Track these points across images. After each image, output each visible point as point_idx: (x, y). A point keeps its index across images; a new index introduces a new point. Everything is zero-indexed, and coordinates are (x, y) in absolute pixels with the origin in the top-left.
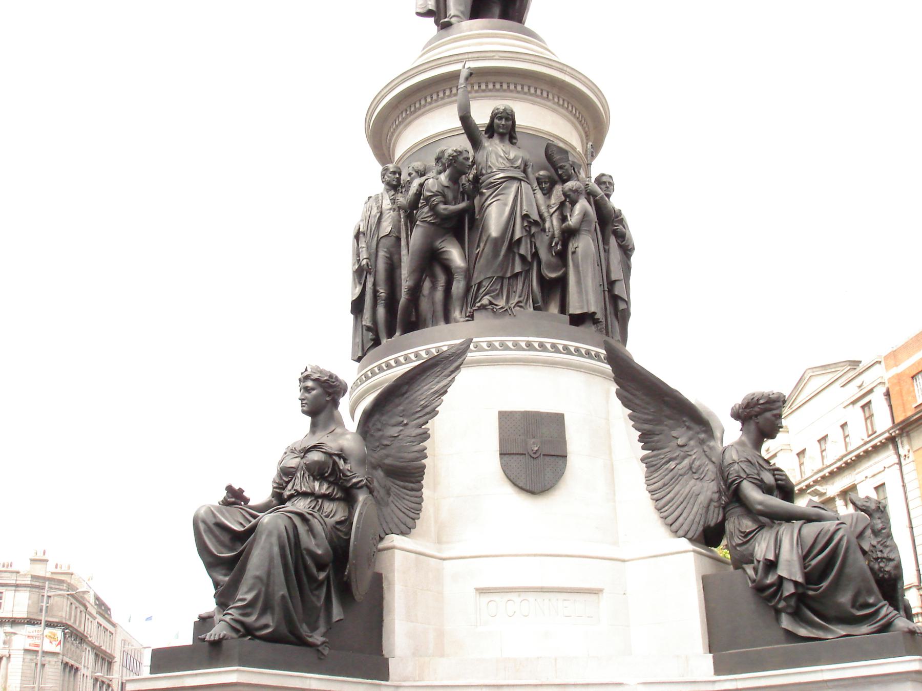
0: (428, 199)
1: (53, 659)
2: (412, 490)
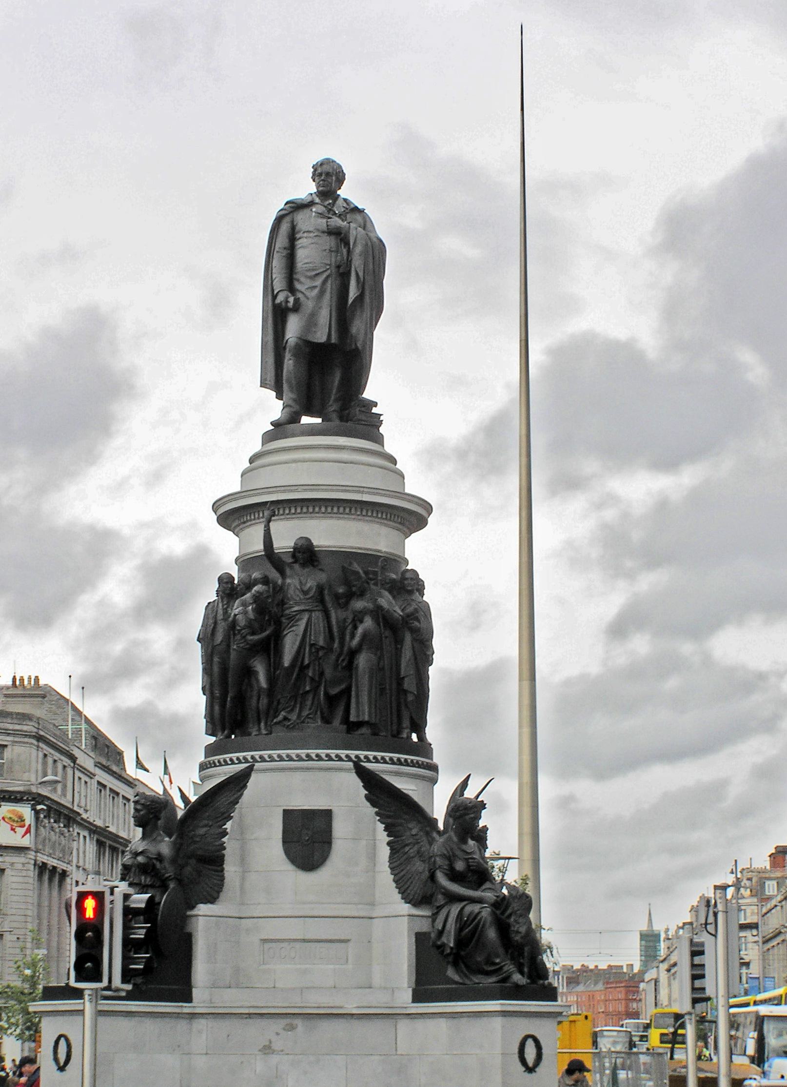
0: (239, 631)
1: (18, 860)
2: (217, 871)
